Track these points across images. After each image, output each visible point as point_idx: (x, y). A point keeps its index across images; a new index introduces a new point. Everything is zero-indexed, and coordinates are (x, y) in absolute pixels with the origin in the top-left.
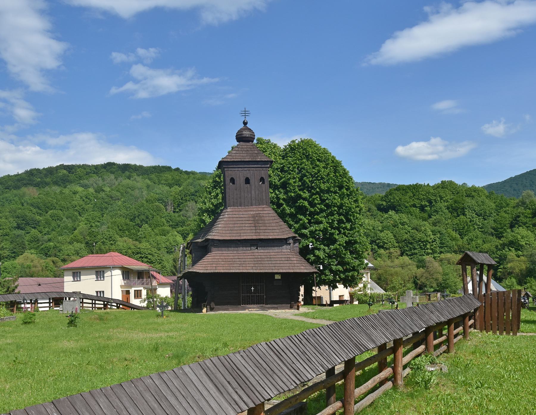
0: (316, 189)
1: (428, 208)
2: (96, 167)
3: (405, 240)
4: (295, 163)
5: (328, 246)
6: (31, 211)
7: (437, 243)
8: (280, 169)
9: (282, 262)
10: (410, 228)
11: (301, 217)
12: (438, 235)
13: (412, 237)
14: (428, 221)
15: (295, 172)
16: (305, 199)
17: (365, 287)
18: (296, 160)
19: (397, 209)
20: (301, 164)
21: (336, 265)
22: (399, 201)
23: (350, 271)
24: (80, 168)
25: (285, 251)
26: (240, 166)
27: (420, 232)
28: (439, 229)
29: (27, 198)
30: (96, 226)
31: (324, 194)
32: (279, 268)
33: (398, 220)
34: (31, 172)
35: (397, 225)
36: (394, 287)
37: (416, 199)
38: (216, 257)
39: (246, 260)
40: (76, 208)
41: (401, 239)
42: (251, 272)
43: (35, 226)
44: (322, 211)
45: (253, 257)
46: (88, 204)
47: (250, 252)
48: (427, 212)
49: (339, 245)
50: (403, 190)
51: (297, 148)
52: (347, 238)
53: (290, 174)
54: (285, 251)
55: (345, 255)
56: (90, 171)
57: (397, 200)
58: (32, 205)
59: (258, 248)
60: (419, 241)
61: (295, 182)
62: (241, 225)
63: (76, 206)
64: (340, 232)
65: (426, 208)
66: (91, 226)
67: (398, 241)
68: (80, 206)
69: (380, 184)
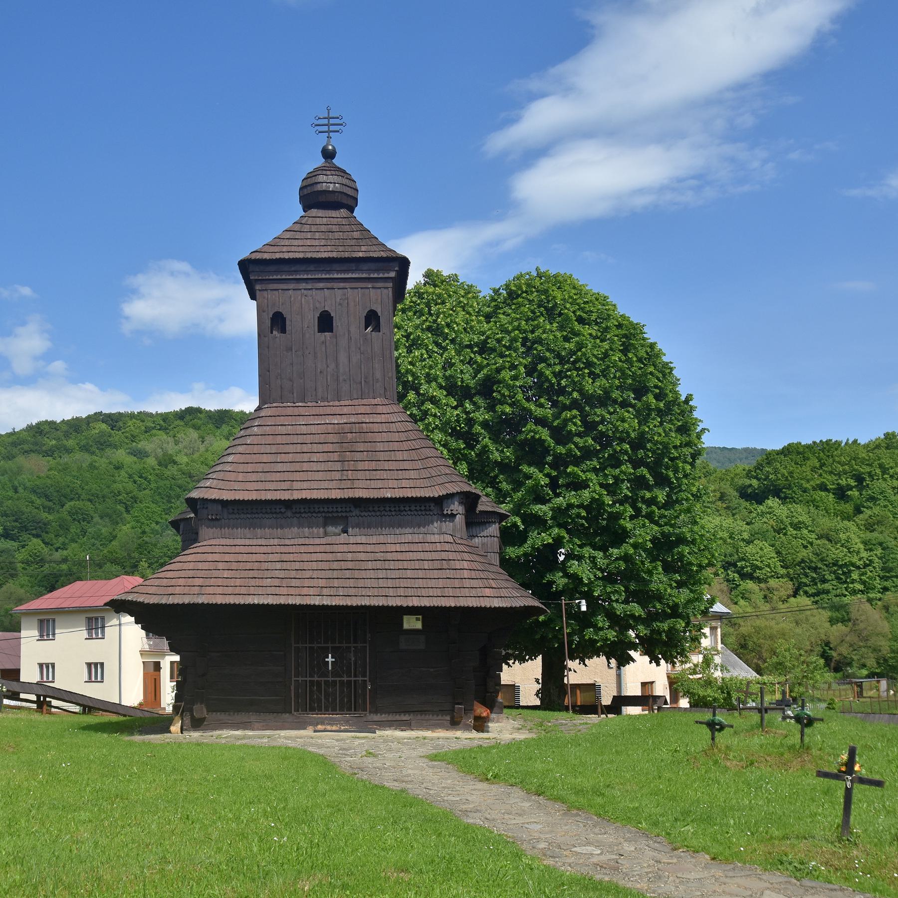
0: (570, 394)
1: (854, 493)
2: (165, 417)
3: (801, 563)
4: (518, 328)
5: (604, 549)
6: (32, 502)
7: (874, 567)
8: (478, 346)
9: (421, 574)
10: (814, 536)
11: (532, 470)
12: (879, 551)
13: (817, 555)
14: (854, 521)
15: (516, 350)
16: (541, 422)
17: (707, 662)
18: (520, 319)
19: (783, 495)
20: (533, 332)
21: (626, 602)
22: (789, 478)
23: (664, 616)
24: (134, 420)
25: (436, 538)
26: (302, 277)
27: (836, 543)
28: (881, 538)
29: (24, 477)
30: (153, 531)
31: (593, 407)
32: (410, 592)
33: (787, 517)
34: (39, 428)
35: (784, 529)
36: (780, 664)
37: (826, 472)
38: (210, 557)
39: (306, 566)
40: (120, 497)
41: (793, 559)
42: (312, 603)
43: (39, 531)
44: (588, 454)
45: (330, 557)
46: (145, 489)
47: (323, 541)
48: (852, 500)
49: (635, 546)
50: (799, 453)
51: (526, 292)
52: (656, 528)
53: (502, 356)
54: (436, 538)
55: (650, 573)
56: (153, 425)
57: (783, 475)
58: (35, 492)
59: (350, 530)
60: (834, 564)
61: (515, 378)
62: (298, 457)
63: (119, 493)
64: (638, 511)
65: (849, 493)
66: (144, 532)
67: (786, 564)
68: (127, 494)
69: (746, 450)
